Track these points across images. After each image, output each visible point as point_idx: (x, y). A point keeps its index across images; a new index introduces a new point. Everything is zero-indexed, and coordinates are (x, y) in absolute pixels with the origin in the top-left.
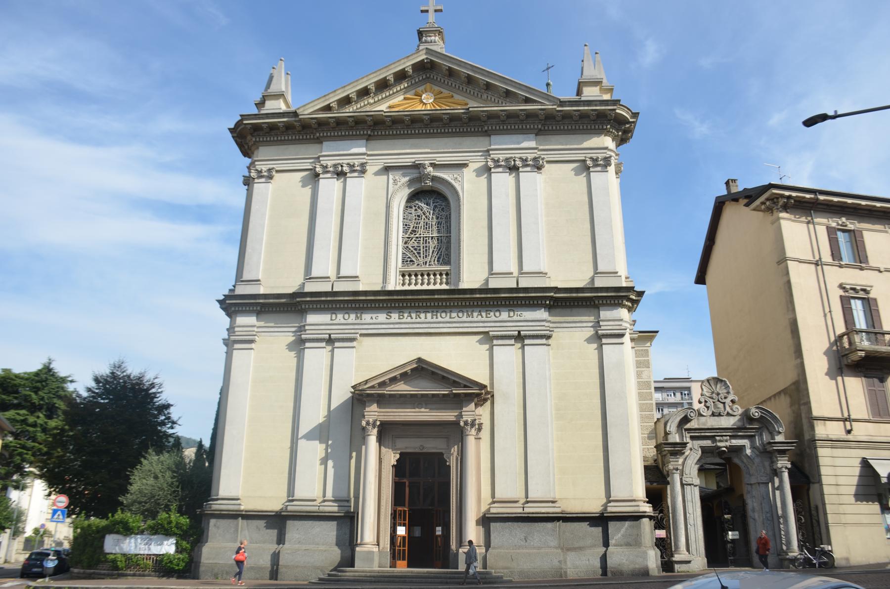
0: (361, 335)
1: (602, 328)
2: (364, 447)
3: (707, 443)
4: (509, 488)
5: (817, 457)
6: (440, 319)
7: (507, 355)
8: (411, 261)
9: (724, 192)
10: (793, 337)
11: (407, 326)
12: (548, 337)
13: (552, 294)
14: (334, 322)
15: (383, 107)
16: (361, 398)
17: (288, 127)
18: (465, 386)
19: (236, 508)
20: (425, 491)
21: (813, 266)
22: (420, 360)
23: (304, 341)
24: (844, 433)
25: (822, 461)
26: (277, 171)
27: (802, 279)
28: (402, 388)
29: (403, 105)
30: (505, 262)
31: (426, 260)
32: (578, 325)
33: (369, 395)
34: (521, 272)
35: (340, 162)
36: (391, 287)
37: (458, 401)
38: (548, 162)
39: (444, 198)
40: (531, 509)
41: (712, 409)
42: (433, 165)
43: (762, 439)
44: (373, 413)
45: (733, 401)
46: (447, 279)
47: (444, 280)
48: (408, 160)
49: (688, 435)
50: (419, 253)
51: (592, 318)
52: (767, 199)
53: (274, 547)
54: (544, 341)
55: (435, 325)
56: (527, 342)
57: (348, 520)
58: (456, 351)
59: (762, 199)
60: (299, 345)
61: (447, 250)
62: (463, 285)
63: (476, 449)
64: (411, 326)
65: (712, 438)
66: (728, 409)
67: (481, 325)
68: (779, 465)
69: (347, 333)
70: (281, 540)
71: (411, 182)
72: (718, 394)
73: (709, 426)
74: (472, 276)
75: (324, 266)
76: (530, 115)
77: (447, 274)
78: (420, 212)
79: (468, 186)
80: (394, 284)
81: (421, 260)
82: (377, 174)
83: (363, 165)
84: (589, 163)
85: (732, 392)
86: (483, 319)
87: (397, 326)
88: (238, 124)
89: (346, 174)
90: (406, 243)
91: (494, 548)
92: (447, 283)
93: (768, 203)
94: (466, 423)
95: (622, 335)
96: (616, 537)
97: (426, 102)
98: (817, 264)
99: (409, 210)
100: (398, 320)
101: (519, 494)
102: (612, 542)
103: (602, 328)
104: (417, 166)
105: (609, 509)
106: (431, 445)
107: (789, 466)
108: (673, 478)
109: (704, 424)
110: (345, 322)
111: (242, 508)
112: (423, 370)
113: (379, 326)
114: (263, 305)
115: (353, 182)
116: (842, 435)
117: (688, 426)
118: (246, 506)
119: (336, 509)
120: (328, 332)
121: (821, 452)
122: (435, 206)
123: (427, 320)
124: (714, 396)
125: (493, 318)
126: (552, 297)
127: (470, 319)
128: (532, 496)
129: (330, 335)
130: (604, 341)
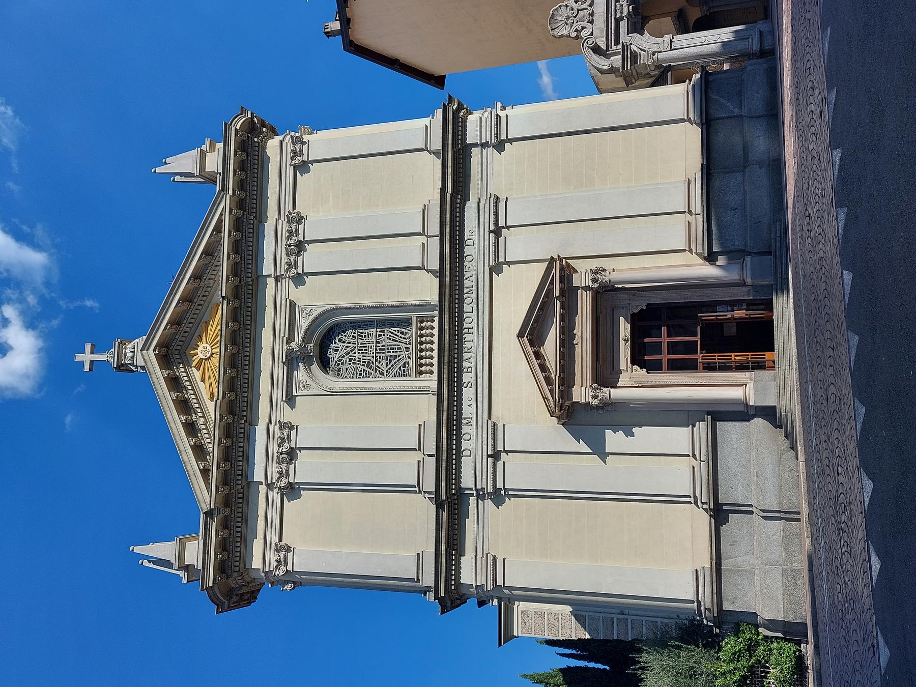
0: (490, 418)
1: (489, 140)
3: (623, 25)
6: (474, 324)
7: (517, 245)
11: (480, 363)
12: (498, 199)
13: (448, 195)
14: (473, 452)
15: (210, 406)
16: (570, 414)
17: (225, 525)
18: (552, 283)
19: (708, 573)
20: (674, 326)
22: (520, 335)
23: (496, 491)
26: (281, 540)
28: (551, 347)
29: (210, 383)
30: (409, 251)
31: (403, 349)
33: (561, 396)
35: (276, 454)
36: (434, 385)
37: (569, 294)
38: (294, 208)
42: (290, 340)
46: (427, 321)
47: (429, 324)
48: (281, 371)
49: (614, 47)
50: (395, 357)
51: (473, 500)
53: (756, 519)
55: (480, 329)
56: (502, 223)
58: (513, 297)
60: (498, 496)
61: (392, 320)
62: (435, 299)
63: (623, 271)
64: (480, 358)
65: (617, 21)
66: (585, 6)
69: (484, 436)
70: (745, 510)
71: (308, 363)
72: (568, 17)
73: (604, 26)
74: (426, 290)
75: (403, 469)
76: (237, 225)
77: (422, 322)
78: (346, 359)
79: (314, 298)
80: (431, 382)
82: (292, 406)
83: (282, 426)
84: (298, 160)
86: (475, 275)
87: (480, 375)
88: (214, 599)
90: (382, 374)
91: (746, 246)
92: (433, 321)
94: (595, 281)
95: (498, 117)
97: (209, 349)
99: (342, 372)
100: (473, 375)
103: (489, 140)
104: (291, 361)
108: (665, 61)
109: (602, 31)
110: (473, 438)
111: (708, 565)
112: (532, 333)
113: (480, 395)
115: (302, 439)
117: (604, 47)
118: (704, 560)
123: (475, 340)
124: (570, 21)
125: (474, 262)
126: (452, 195)
127: (474, 290)
129: (489, 456)
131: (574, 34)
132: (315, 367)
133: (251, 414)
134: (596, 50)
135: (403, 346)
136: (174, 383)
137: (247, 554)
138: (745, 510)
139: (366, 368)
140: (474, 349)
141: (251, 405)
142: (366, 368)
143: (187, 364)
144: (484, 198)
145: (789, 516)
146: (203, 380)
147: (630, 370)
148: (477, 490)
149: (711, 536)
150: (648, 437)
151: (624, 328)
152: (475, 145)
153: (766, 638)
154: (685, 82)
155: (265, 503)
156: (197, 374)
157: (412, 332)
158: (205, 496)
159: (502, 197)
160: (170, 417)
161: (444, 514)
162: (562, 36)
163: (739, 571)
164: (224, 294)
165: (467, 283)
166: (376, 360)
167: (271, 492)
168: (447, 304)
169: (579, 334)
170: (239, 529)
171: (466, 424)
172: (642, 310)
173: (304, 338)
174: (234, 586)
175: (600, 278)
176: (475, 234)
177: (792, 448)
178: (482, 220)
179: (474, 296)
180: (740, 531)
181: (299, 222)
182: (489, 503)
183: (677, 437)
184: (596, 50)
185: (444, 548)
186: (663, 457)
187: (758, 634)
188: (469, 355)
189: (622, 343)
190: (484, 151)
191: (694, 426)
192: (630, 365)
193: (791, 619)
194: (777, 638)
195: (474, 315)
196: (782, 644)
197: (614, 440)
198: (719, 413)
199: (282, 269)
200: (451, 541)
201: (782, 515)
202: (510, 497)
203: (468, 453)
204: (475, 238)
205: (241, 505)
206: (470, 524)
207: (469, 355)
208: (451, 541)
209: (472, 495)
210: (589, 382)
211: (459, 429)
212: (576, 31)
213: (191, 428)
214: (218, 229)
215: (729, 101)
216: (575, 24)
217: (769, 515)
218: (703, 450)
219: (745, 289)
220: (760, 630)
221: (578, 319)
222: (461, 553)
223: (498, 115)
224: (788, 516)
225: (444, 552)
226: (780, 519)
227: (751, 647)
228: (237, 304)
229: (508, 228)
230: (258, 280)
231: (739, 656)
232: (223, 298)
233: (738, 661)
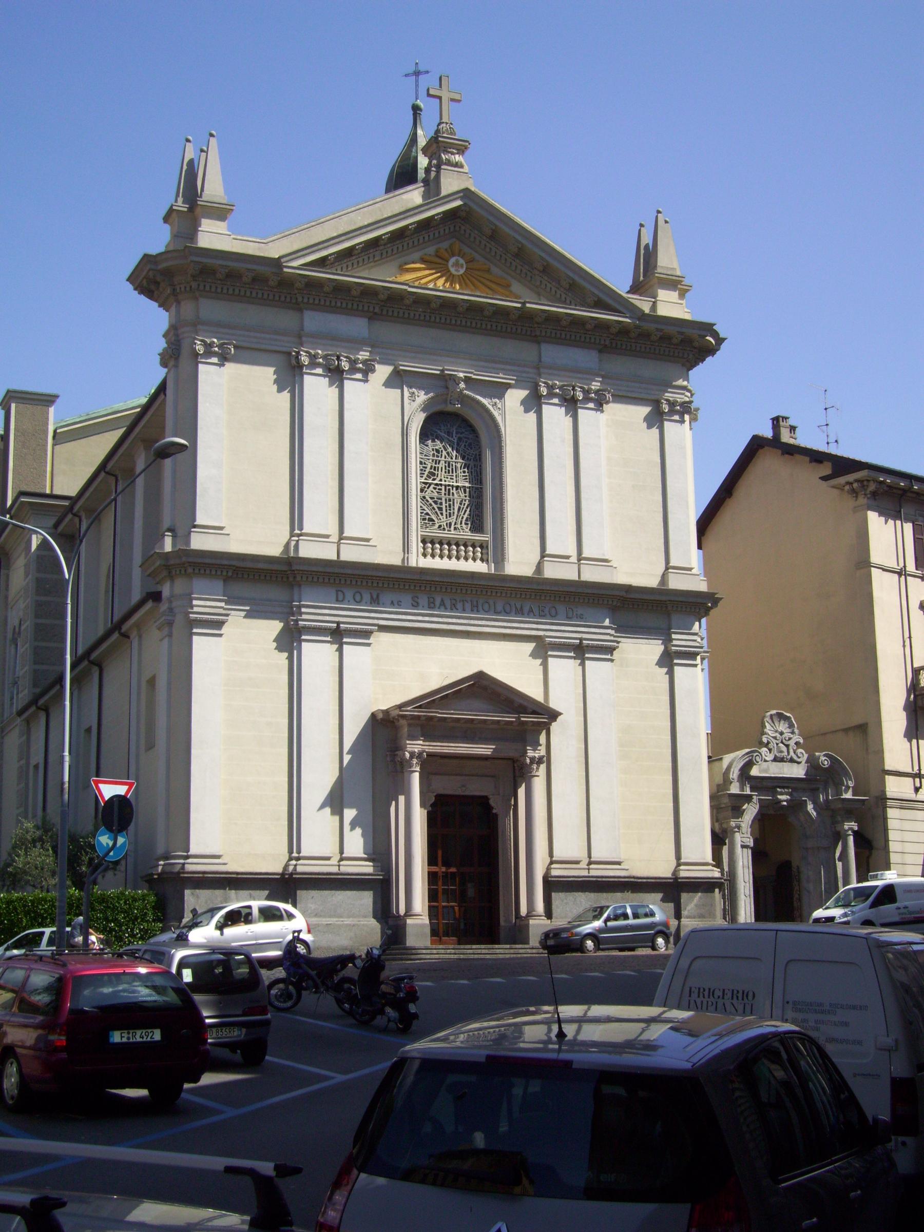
4: (569, 845)
5: (885, 819)
7: (563, 669)
8: (431, 520)
9: (768, 433)
20: (473, 841)
21: (896, 576)
24: (912, 791)
25: (892, 824)
27: (884, 589)
30: (561, 541)
31: (450, 520)
39: (472, 429)
40: (597, 872)
41: (775, 752)
43: (827, 796)
45: (797, 743)
46: (482, 553)
50: (440, 509)
52: (856, 481)
57: (382, 887)
58: (509, 663)
59: (851, 477)
60: (290, 640)
61: (482, 507)
66: (792, 753)
68: (846, 827)
74: (520, 561)
75: (319, 516)
79: (510, 412)
81: (444, 520)
85: (796, 731)
89: (343, 371)
93: (855, 485)
96: (689, 908)
98: (900, 574)
101: (582, 854)
102: (684, 913)
105: (683, 874)
106: (475, 788)
107: (856, 828)
112: (481, 687)
116: (911, 795)
119: (370, 870)
120: (337, 619)
121: (891, 813)
122: (460, 439)
124: (778, 735)
128: (595, 856)
131: (765, 740)
134: (749, 765)
135: (453, 519)
139: (428, 470)
142: (428, 470)
154: (713, 860)
157: (466, 533)
162: (764, 726)
164: (528, 305)
166: (437, 484)
175: (535, 766)
184: (749, 765)
212: (768, 743)
215: (696, 905)
216: (774, 741)
218: (350, 868)
223: (697, 654)
232: (524, 303)
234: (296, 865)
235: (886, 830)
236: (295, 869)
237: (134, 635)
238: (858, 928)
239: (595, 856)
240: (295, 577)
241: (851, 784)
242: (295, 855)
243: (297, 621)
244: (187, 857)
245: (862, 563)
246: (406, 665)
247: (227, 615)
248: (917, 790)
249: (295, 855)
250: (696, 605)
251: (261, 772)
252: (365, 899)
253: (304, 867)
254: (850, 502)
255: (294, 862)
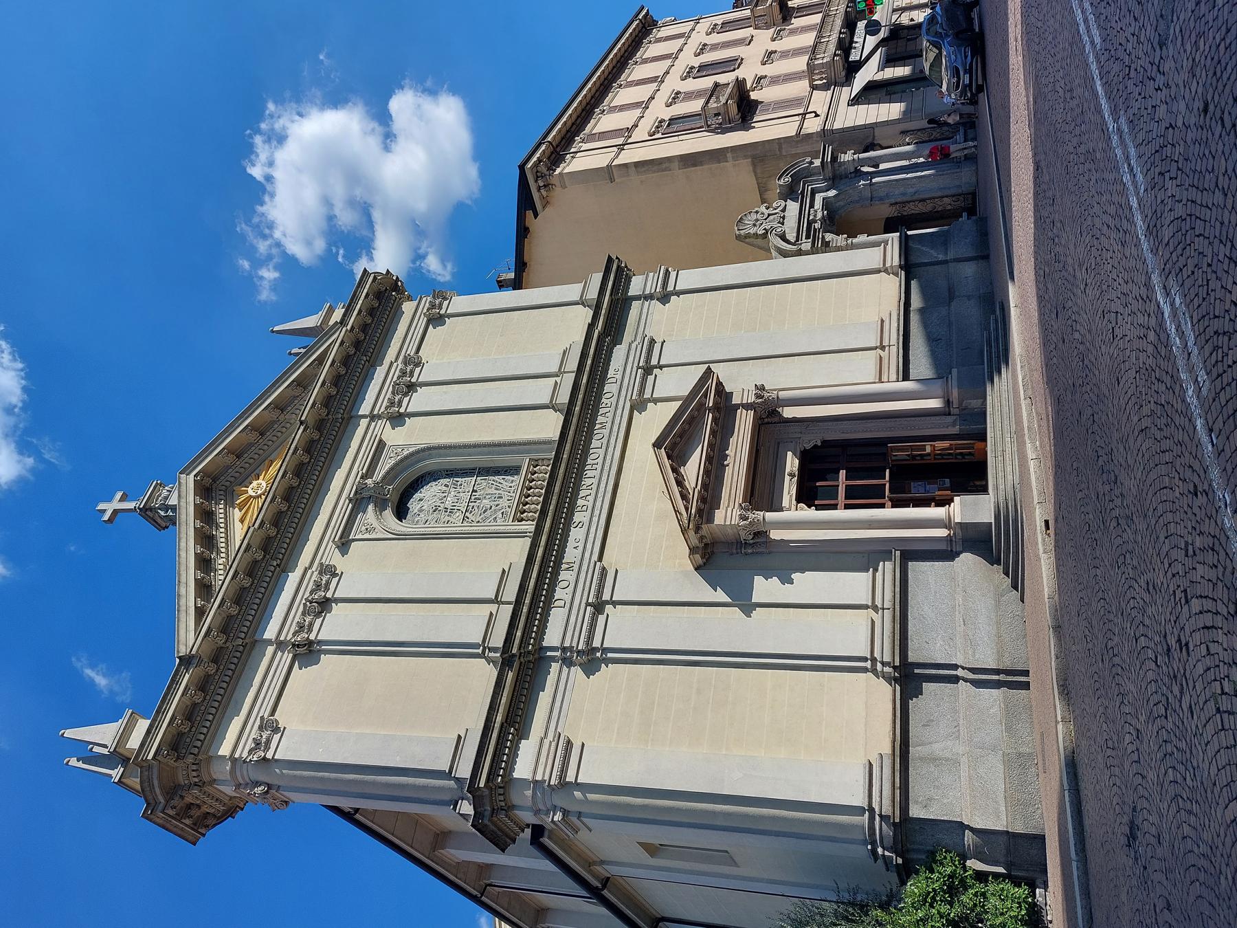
0: (600, 558)
2: (788, 412)
5: (843, 130)
10: (701, 164)
17: (203, 685)
18: (705, 395)
22: (657, 445)
28: (693, 469)
30: (540, 391)
32: (644, 317)
34: (496, 600)
44: (728, 514)
48: (345, 507)
51: (555, 667)
52: (536, 181)
54: (657, 347)
59: (536, 195)
60: (591, 659)
64: (600, 495)
67: (619, 412)
70: (946, 675)
71: (381, 506)
74: (549, 426)
76: (346, 360)
80: (530, 527)
103: (574, 644)
104: (359, 502)
112: (674, 446)
114: (509, 721)
120: (583, 605)
130: (570, 777)
132: (388, 513)
133: (288, 560)
136: (206, 515)
137: (217, 733)
138: (946, 675)
140: (594, 487)
141: (293, 549)
143: (230, 503)
144: (639, 339)
145: (1011, 679)
146: (242, 521)
147: (793, 507)
148: (564, 649)
149: (894, 709)
150: (808, 585)
151: (792, 463)
152: (637, 298)
153: (981, 877)
154: (867, 571)
155: (270, 665)
156: (237, 514)
158: (188, 637)
159: (659, 340)
160: (183, 544)
161: (510, 674)
163: (935, 759)
165: (600, 419)
167: (279, 654)
168: (571, 433)
169: (732, 454)
170: (219, 698)
171: (567, 569)
172: (815, 446)
173: (384, 477)
174: (181, 792)
175: (766, 395)
176: (620, 373)
177: (1015, 587)
178: (631, 359)
179: (606, 432)
180: (938, 706)
181: (417, 365)
182: (577, 672)
183: (853, 585)
185: (499, 718)
186: (830, 611)
187: (965, 868)
188: (588, 492)
189: (787, 478)
190: (647, 303)
191: (876, 570)
192: (794, 502)
193: (1019, 828)
194: (996, 876)
195: (601, 452)
196: (1007, 886)
197: (765, 588)
198: (911, 553)
199: (381, 408)
200: (510, 716)
201: (1002, 677)
202: (608, 661)
203: (561, 603)
204: (619, 376)
205: (233, 667)
206: (544, 699)
207: (588, 492)
208: (510, 716)
209: (553, 659)
210: (740, 499)
211: (556, 573)
213: (204, 564)
214: (321, 360)
217: (985, 678)
218: (887, 596)
219: (949, 419)
220: (969, 863)
221: (733, 441)
222: (523, 734)
224: (1010, 678)
225: (497, 725)
226: (998, 685)
227: (953, 889)
228: (316, 436)
229: (661, 367)
230: (349, 420)
231: (933, 898)
233: (931, 906)
234: (883, 663)
235: (854, 128)
236: (888, 664)
237: (602, 871)
238: (1014, 371)
239: (874, 342)
240: (529, 652)
241: (808, 159)
242: (868, 664)
243: (579, 652)
244: (871, 810)
245: (609, 173)
246: (639, 523)
247: (569, 743)
248: (817, 115)
249: (868, 664)
250: (617, 276)
251: (758, 705)
252: (921, 571)
253: (885, 651)
254: (557, 192)
255: (879, 667)
